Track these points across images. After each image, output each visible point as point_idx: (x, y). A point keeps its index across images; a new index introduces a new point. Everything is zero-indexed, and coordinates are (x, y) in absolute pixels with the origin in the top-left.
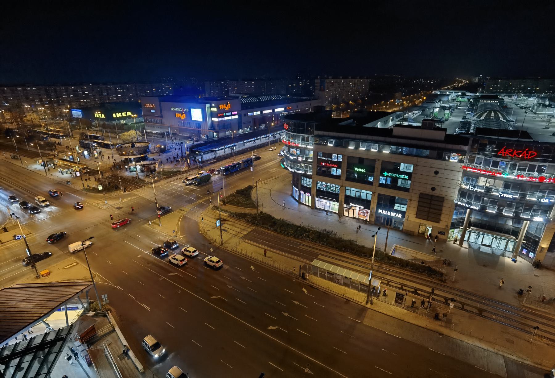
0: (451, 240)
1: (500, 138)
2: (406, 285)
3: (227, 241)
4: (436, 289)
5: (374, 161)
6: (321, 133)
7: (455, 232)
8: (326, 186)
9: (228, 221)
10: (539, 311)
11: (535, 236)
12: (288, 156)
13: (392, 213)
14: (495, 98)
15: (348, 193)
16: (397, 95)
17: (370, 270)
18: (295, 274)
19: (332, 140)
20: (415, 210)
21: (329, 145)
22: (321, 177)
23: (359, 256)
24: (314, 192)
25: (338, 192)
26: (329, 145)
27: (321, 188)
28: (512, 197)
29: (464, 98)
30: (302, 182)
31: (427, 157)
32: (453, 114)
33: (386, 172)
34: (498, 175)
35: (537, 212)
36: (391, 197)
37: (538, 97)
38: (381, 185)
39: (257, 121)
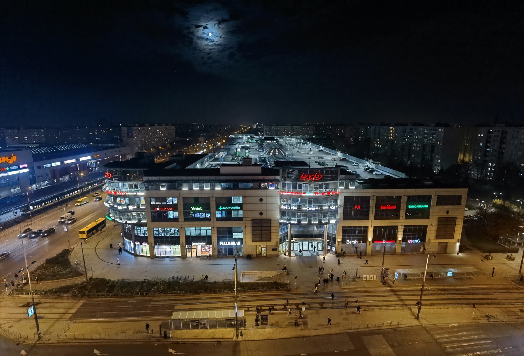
3: (47, 330)
4: (289, 299)
5: (209, 198)
6: (151, 178)
7: (283, 246)
8: (164, 231)
9: (41, 303)
10: (352, 288)
12: (116, 206)
14: (273, 139)
15: (188, 233)
16: (201, 139)
17: (235, 302)
18: (154, 337)
19: (164, 184)
20: (251, 235)
21: (161, 189)
22: (158, 223)
23: (215, 292)
24: (151, 240)
25: (178, 234)
26: (161, 189)
29: (253, 140)
31: (251, 188)
32: (250, 152)
33: (221, 207)
34: (304, 194)
37: (296, 138)
38: (218, 219)
39: (55, 173)
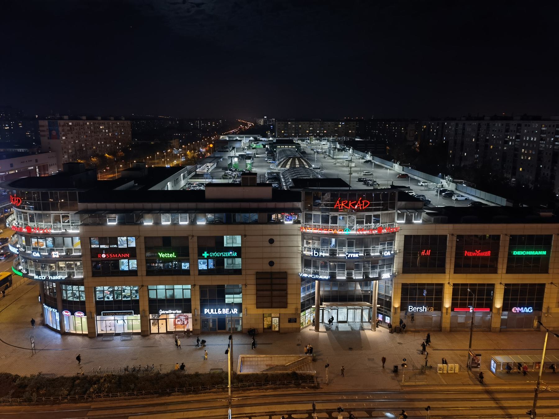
0: (305, 326)
1: (320, 188)
2: (274, 412)
5: (186, 238)
7: (306, 315)
11: (386, 296)
13: (223, 309)
14: (291, 142)
15: (153, 295)
19: (113, 215)
20: (254, 297)
23: (196, 392)
24: (91, 307)
25: (136, 296)
27: (104, 297)
28: (358, 255)
29: (259, 144)
30: (65, 295)
31: (256, 222)
32: (254, 164)
33: (206, 252)
35: (382, 268)
36: (219, 286)
37: (328, 141)
38: (202, 272)
